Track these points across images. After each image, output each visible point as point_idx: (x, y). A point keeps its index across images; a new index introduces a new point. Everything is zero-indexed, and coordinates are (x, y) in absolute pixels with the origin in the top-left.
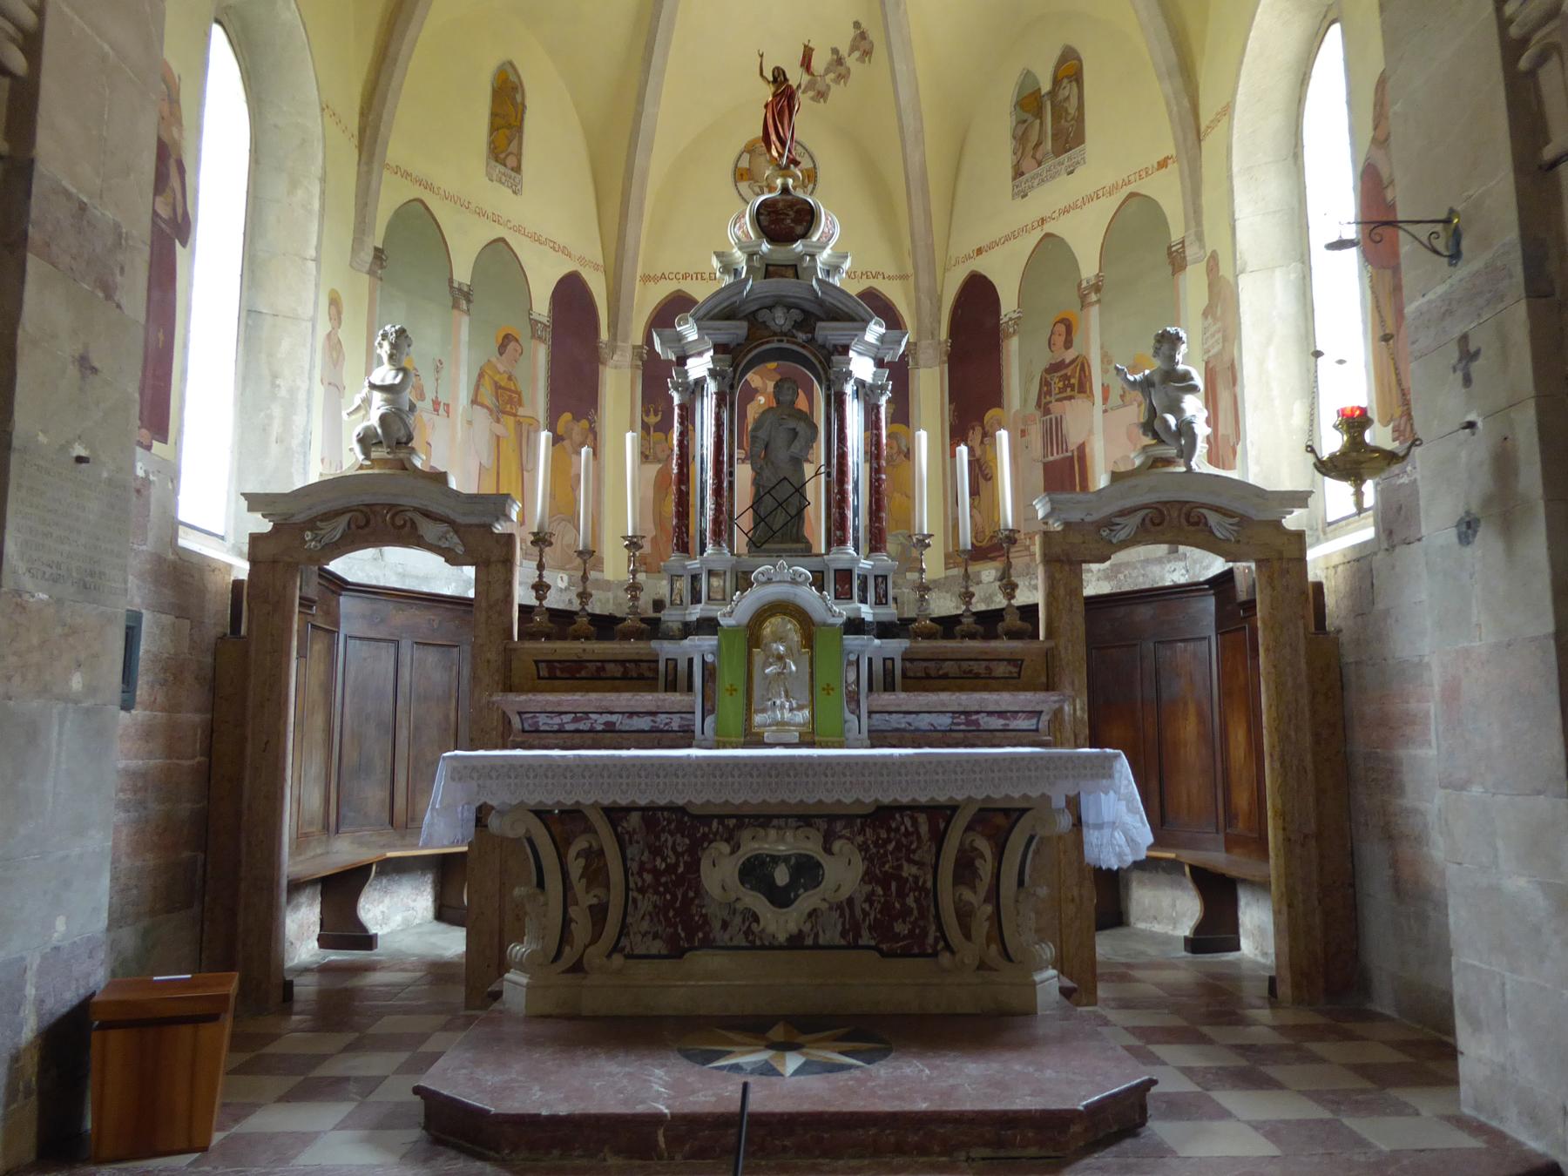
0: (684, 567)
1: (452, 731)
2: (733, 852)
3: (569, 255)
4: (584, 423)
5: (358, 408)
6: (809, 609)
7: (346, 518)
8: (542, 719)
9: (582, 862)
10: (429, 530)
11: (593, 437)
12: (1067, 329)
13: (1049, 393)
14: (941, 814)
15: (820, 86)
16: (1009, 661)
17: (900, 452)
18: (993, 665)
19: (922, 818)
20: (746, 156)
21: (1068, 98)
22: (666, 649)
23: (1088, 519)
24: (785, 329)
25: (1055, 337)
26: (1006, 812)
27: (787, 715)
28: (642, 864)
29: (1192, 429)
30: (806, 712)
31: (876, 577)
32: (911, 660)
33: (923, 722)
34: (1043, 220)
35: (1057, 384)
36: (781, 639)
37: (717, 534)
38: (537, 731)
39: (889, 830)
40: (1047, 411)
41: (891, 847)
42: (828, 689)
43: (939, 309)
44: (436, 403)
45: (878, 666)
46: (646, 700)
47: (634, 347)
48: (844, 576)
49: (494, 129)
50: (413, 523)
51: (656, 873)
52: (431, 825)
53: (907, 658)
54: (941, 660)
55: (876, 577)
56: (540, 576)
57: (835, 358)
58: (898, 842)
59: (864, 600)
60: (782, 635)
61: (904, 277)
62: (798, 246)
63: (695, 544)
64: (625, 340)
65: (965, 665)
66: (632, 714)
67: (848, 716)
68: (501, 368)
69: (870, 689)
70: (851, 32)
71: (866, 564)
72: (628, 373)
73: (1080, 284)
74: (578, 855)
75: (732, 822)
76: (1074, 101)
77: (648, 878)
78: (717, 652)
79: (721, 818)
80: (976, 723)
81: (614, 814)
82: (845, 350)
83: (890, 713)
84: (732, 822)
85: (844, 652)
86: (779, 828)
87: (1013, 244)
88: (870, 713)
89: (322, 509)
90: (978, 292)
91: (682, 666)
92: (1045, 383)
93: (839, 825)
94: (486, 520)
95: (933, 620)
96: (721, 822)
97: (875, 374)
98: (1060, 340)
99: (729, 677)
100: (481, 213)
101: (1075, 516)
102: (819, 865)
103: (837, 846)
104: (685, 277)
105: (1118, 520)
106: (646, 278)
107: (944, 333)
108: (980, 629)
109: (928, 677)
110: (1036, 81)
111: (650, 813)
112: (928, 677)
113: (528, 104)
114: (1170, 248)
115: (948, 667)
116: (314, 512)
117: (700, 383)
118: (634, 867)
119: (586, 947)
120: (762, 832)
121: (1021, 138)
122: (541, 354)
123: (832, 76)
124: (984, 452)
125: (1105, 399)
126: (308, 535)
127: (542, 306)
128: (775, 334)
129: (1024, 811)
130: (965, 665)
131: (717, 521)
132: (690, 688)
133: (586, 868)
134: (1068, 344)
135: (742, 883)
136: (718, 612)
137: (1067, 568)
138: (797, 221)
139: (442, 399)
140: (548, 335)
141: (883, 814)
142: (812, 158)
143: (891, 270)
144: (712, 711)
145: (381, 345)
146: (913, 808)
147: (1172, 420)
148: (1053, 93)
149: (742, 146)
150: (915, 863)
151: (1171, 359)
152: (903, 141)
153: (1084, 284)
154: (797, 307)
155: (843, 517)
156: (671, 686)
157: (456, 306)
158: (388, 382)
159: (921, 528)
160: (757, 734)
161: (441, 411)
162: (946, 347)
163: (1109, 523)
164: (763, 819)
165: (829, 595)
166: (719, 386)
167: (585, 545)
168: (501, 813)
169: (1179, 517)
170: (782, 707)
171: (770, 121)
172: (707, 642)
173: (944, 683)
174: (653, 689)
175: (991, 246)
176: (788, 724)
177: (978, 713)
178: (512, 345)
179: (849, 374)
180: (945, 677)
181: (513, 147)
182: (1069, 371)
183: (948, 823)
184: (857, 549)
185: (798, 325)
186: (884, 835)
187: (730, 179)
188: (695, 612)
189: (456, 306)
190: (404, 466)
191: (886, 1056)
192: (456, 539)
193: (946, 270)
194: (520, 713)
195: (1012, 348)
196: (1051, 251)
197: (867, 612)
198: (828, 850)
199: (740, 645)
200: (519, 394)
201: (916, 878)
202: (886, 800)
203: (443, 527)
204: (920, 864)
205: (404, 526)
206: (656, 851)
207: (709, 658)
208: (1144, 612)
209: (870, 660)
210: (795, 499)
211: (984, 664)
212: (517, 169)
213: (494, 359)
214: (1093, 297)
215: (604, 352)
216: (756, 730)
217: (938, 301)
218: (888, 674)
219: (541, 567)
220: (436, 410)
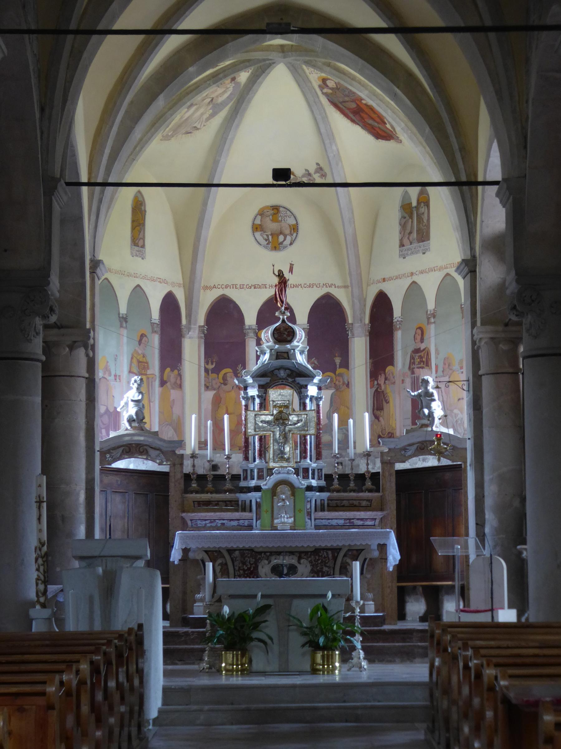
0: (248, 466)
1: (126, 533)
2: (269, 564)
3: (167, 283)
4: (176, 372)
5: (123, 406)
6: (293, 482)
7: (122, 448)
8: (199, 522)
9: (220, 567)
10: (153, 453)
11: (180, 386)
12: (421, 333)
13: (414, 363)
14: (336, 551)
16: (367, 500)
17: (344, 383)
19: (330, 552)
20: (259, 217)
21: (423, 213)
22: (242, 497)
23: (397, 447)
24: (284, 377)
25: (417, 335)
26: (357, 550)
27: (286, 520)
28: (239, 567)
29: (433, 415)
30: (293, 519)
31: (318, 470)
32: (331, 500)
33: (334, 522)
34: (412, 274)
35: (417, 360)
36: (284, 494)
37: (260, 455)
39: (319, 556)
40: (413, 373)
41: (319, 562)
42: (300, 511)
43: (365, 306)
44: (115, 376)
45: (319, 502)
46: (237, 515)
47: (200, 327)
48: (306, 470)
49: (133, 228)
50: (146, 450)
51: (244, 570)
52: (175, 554)
53: (329, 499)
55: (318, 470)
57: (303, 390)
58: (322, 560)
59: (313, 478)
60: (284, 493)
61: (346, 287)
62: (288, 346)
63: (251, 458)
64: (195, 324)
65: (351, 502)
66: (231, 520)
67: (307, 520)
68: (140, 352)
69: (316, 510)
70: (315, 166)
71: (314, 465)
72: (196, 341)
73: (427, 312)
74: (219, 565)
75: (268, 554)
76: (426, 215)
77: (241, 572)
78: (261, 498)
79: (265, 552)
80: (353, 522)
81: (230, 551)
82: (306, 387)
83: (322, 519)
84: (268, 554)
85: (306, 497)
86: (283, 556)
88: (315, 519)
89: (113, 446)
90: (382, 303)
91: (248, 502)
92: (412, 358)
93: (303, 555)
96: (265, 554)
97: (318, 393)
98: (419, 337)
99: (265, 507)
100: (129, 275)
101: (392, 446)
102: (296, 567)
103: (302, 561)
104: (227, 287)
105: (408, 448)
106: (206, 288)
107: (367, 320)
108: (356, 488)
109: (337, 506)
110: (410, 198)
111: (242, 551)
112: (337, 506)
113: (147, 209)
114: (461, 305)
116: (109, 448)
117: (253, 398)
118: (237, 568)
120: (278, 557)
121: (403, 226)
122: (156, 340)
124: (386, 388)
125: (436, 371)
126: (108, 456)
127: (156, 315)
128: (280, 379)
129: (363, 550)
130: (351, 502)
131: (260, 451)
132: (251, 511)
133: (221, 569)
134: (422, 340)
135: (272, 573)
136: (262, 483)
137: (389, 465)
138: (288, 335)
139: (118, 374)
140: (158, 329)
141: (317, 551)
142: (295, 218)
143: (339, 283)
144: (259, 519)
145: (133, 384)
146: (326, 549)
147: (426, 411)
148: (417, 208)
150: (327, 567)
151: (426, 388)
152: (343, 222)
153: (429, 313)
154: (289, 369)
155: (306, 449)
156: (244, 510)
157: (121, 326)
158: (136, 398)
159: (335, 451)
160: (275, 527)
161: (118, 380)
162: (368, 327)
163: (405, 449)
164: (278, 553)
165: (300, 478)
166: (260, 401)
167: (210, 458)
168: (194, 551)
169: (423, 448)
170: (284, 517)
171: (277, 293)
172: (258, 494)
173: (344, 508)
174: (237, 511)
175: (390, 279)
176: (286, 523)
177: (353, 519)
178: (144, 339)
179: (308, 396)
180: (343, 506)
181: (141, 236)
182: (422, 354)
183: (338, 554)
184: (311, 460)
185: (289, 376)
186: (317, 558)
187: (250, 230)
188: (253, 483)
189: (121, 326)
190: (142, 429)
193: (368, 285)
194: (191, 520)
195: (398, 335)
196: (414, 291)
197: (314, 483)
198: (299, 563)
199: (269, 495)
200: (147, 363)
201: (328, 572)
202: (317, 545)
204: (329, 567)
205: (143, 451)
206: (244, 563)
207: (258, 500)
208: (448, 476)
209: (316, 500)
210: (276, 336)
211: (358, 501)
212: (143, 246)
213: (137, 348)
214: (432, 320)
215: (184, 330)
216: (275, 525)
217: (363, 301)
218: (322, 505)
220: (116, 379)
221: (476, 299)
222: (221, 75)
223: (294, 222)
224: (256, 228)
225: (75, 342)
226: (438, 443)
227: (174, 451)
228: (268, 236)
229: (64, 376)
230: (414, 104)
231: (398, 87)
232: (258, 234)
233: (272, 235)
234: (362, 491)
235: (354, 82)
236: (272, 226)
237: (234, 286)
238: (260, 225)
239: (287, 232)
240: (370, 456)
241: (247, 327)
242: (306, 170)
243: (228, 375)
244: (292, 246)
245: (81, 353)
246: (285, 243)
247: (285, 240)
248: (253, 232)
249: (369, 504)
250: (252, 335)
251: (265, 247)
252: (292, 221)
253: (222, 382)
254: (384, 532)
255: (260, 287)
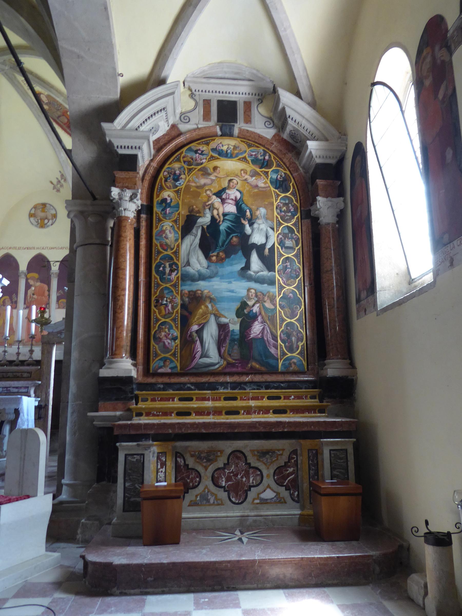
16: (28, 372)
18: (23, 374)
20: (33, 210)
23: (54, 331)
54: (7, 372)
65: (15, 374)
70: (60, 174)
80: (10, 390)
87: (32, 250)
95: (7, 361)
104: (10, 248)
115: (10, 375)
119: (424, 599)
130: (15, 374)
177: (10, 387)
180: (9, 377)
191: (364, 584)
226: (41, 315)
230: (39, 34)
231: (22, 16)
232: (32, 219)
233: (41, 219)
234: (12, 366)
235: (52, 90)
236: (41, 214)
237: (15, 248)
239: (50, 217)
240: (34, 338)
241: (20, 272)
243: (6, 301)
248: (29, 219)
249: (29, 375)
250: (23, 276)
251: (36, 226)
252: (53, 212)
253: (2, 304)
254: (15, 398)
255: (31, 249)
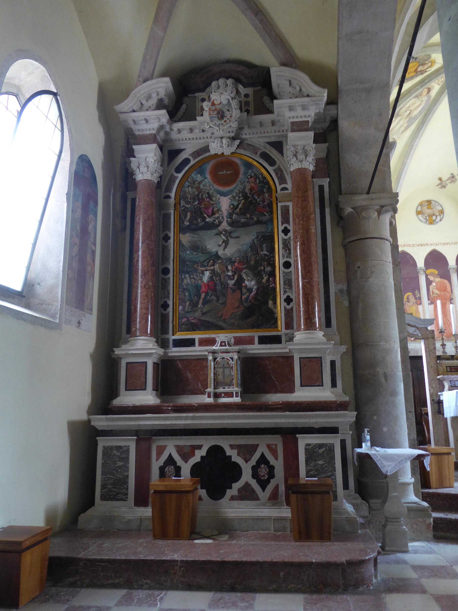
15: (444, 184)
20: (420, 207)
38: (455, 386)
56: (443, 342)
94: (427, 326)
104: (404, 246)
123: (449, 181)
142: (441, 206)
149: (417, 204)
167: (455, 333)
187: (415, 214)
192: (418, 332)
203: (414, 329)
209: (333, 363)
219: (443, 339)
221: (111, 436)
222: (427, 80)
223: (441, 209)
224: (418, 213)
225: (382, 207)
227: (426, 328)
228: (426, 217)
229: (374, 238)
232: (420, 216)
236: (428, 211)
238: (421, 211)
239: (437, 214)
242: (452, 174)
243: (410, 297)
244: (441, 222)
245: (387, 217)
246: (436, 220)
247: (436, 218)
250: (422, 272)
252: (440, 208)
253: (406, 300)
255: (424, 245)
